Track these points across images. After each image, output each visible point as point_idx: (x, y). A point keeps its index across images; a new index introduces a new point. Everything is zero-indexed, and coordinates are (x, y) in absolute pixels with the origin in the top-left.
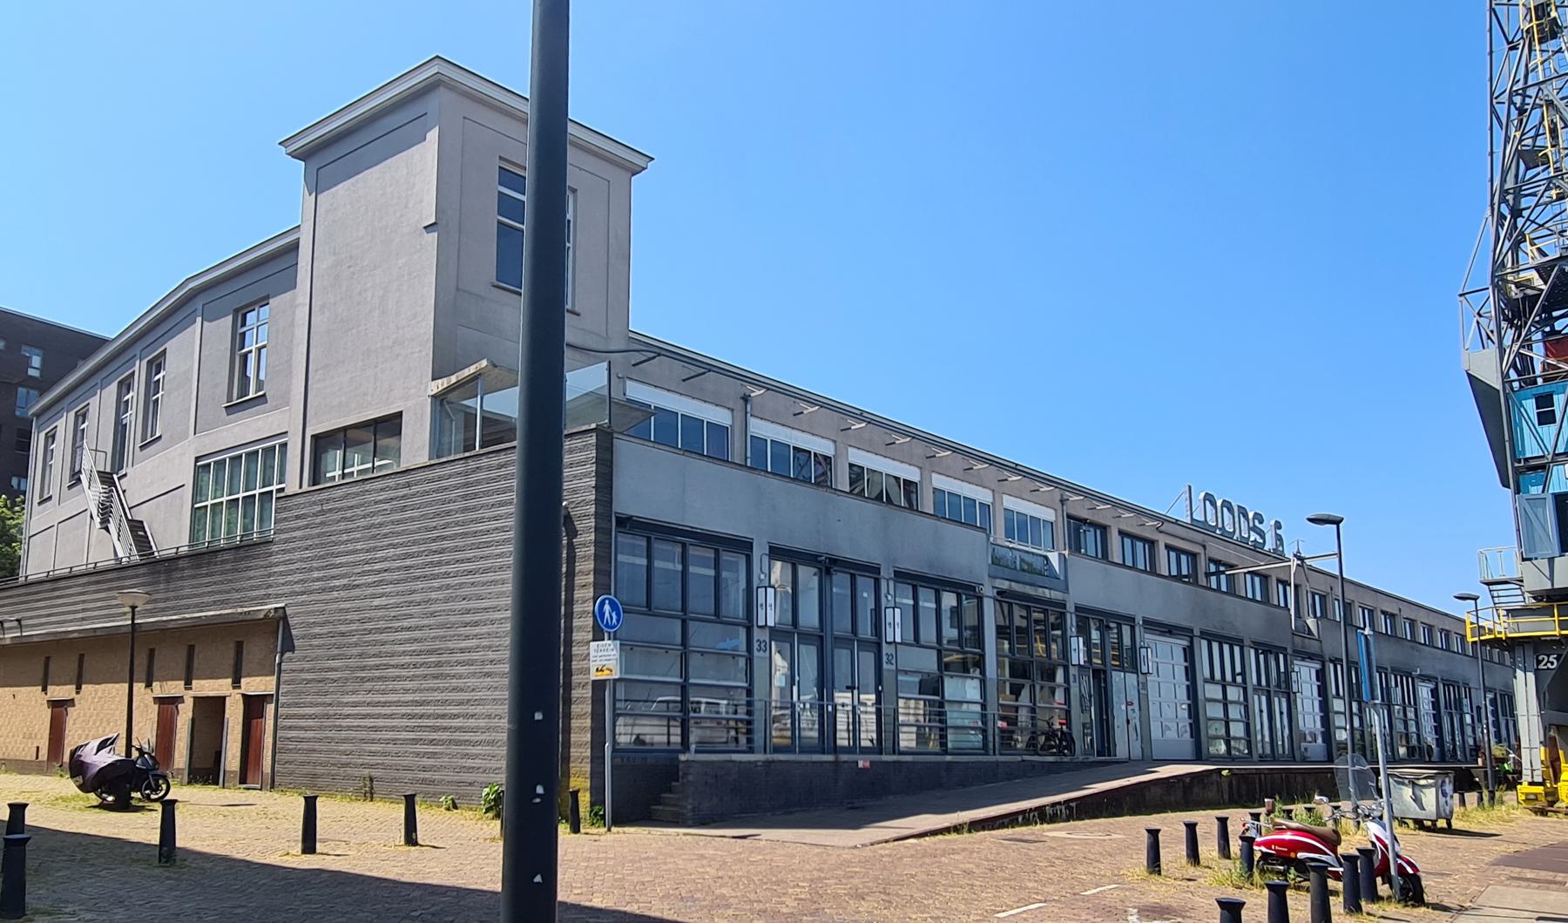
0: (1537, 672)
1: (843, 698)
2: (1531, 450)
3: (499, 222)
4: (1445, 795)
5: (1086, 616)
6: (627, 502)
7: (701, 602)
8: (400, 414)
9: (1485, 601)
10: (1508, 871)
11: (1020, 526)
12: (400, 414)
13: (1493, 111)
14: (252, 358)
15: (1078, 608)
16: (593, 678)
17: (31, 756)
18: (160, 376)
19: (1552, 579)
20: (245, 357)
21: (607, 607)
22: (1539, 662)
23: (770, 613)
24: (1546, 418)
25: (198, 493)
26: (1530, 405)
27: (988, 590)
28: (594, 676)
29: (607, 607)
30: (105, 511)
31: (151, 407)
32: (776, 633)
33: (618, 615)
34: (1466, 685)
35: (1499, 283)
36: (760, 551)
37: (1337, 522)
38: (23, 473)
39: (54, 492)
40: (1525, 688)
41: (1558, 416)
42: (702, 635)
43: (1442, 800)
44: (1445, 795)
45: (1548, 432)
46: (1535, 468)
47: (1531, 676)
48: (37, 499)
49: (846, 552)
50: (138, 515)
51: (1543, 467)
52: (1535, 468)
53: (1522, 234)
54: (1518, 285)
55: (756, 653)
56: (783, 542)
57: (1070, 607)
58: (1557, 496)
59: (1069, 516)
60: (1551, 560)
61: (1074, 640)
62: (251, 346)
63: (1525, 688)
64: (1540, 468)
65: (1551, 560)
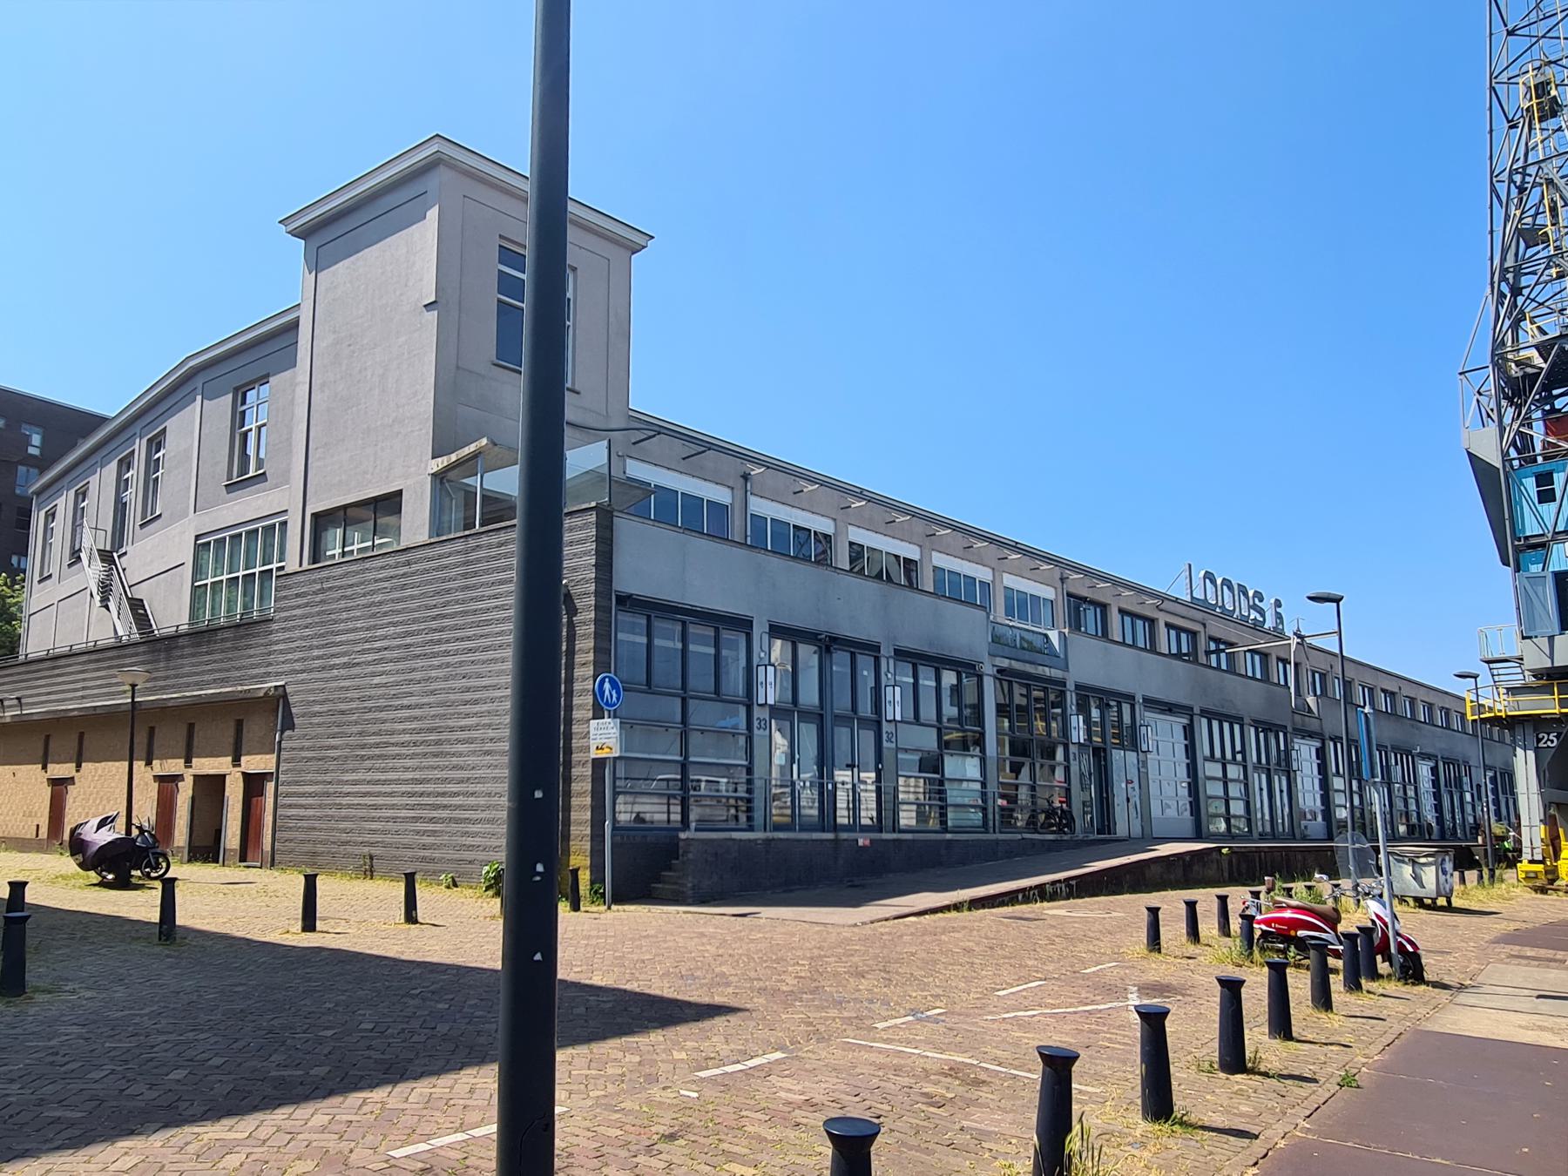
0: (1537, 750)
1: (843, 776)
2: (1531, 528)
3: (499, 301)
4: (1444, 873)
5: (1086, 694)
6: (626, 582)
7: (701, 680)
8: (400, 492)
9: (1485, 679)
10: (1509, 949)
11: (1020, 605)
12: (400, 492)
13: (1493, 190)
14: (252, 436)
15: (1078, 687)
16: (593, 756)
17: (31, 834)
18: (160, 454)
19: (1552, 657)
20: (245, 435)
21: (607, 686)
22: (1539, 740)
23: (770, 691)
24: (1546, 496)
25: (198, 571)
26: (1530, 484)
27: (987, 669)
28: (594, 754)
29: (607, 686)
30: (105, 590)
31: (151, 486)
32: (776, 711)
33: (618, 693)
34: (1466, 763)
35: (1499, 361)
36: (760, 630)
37: (1337, 600)
38: (23, 552)
39: (54, 570)
40: (1525, 766)
41: (1558, 495)
42: (702, 714)
43: (1442, 878)
44: (1444, 873)
45: (1548, 510)
46: (1534, 547)
47: (1531, 754)
48: (37, 578)
49: (846, 630)
50: (138, 593)
51: (1543, 545)
52: (1534, 547)
53: (1522, 312)
54: (1518, 363)
55: (756, 731)
56: (784, 620)
57: (1070, 686)
58: (1557, 575)
59: (1069, 595)
60: (1551, 638)
61: (1074, 718)
62: (251, 425)
63: (1525, 766)
64: (1540, 546)
65: (1551, 638)
